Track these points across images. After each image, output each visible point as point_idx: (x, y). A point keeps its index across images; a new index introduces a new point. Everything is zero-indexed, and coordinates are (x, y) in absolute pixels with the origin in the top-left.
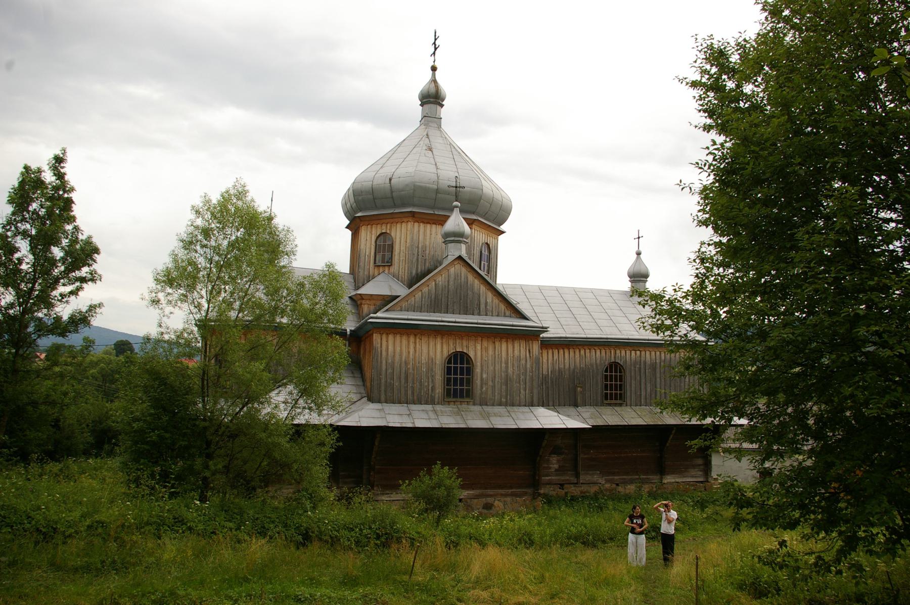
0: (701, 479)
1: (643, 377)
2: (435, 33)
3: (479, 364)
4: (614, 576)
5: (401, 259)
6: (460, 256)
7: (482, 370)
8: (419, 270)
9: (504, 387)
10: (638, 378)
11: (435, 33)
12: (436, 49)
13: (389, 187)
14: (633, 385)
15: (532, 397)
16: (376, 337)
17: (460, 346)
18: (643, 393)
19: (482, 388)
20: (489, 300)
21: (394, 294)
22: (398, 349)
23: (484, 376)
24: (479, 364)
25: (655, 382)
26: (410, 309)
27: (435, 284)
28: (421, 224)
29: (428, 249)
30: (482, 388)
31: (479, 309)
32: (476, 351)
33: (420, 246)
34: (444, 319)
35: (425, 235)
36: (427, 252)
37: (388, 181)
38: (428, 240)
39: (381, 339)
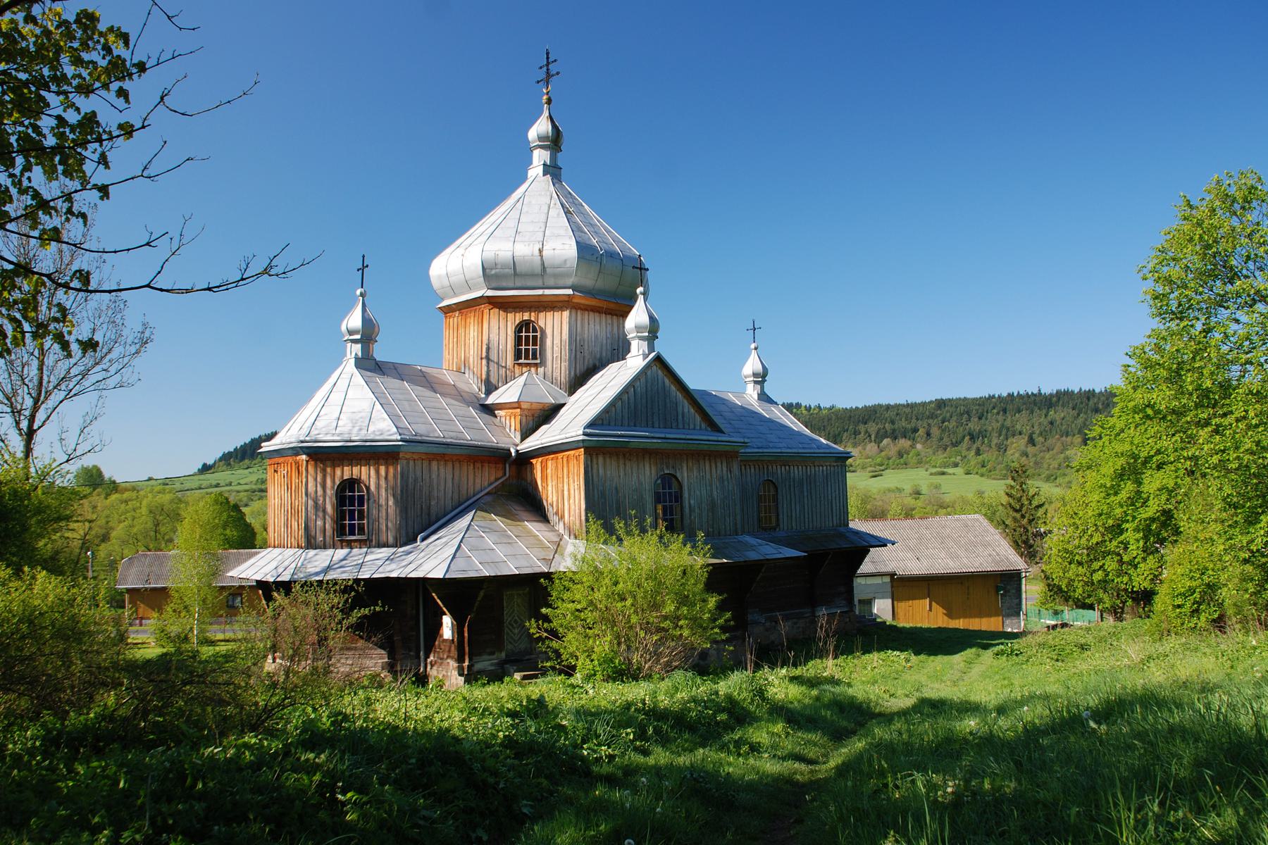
2: (548, 54)
3: (686, 484)
4: (759, 743)
5: (555, 356)
7: (690, 495)
8: (578, 371)
9: (710, 514)
11: (548, 54)
12: (549, 75)
13: (511, 253)
15: (736, 524)
16: (537, 463)
17: (347, 472)
18: (794, 515)
19: (690, 516)
20: (686, 410)
23: (692, 502)
24: (686, 484)
26: (613, 423)
29: (586, 343)
30: (690, 516)
32: (687, 475)
33: (578, 338)
36: (586, 347)
38: (586, 332)
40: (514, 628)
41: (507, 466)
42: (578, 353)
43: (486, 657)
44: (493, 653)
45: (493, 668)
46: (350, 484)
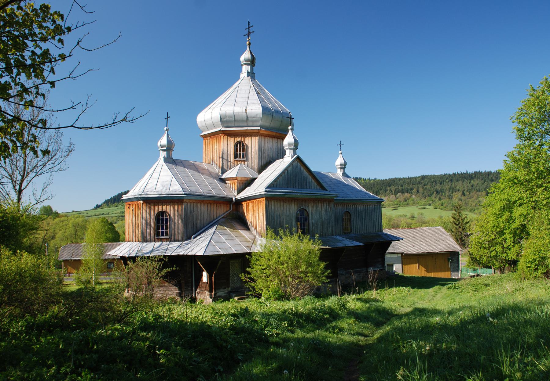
0: (381, 269)
1: (358, 220)
2: (249, 23)
4: (343, 328)
6: (46, 120)
10: (356, 219)
11: (249, 23)
14: (354, 223)
21: (254, 177)
22: (367, 208)
23: (313, 221)
25: (363, 221)
27: (288, 172)
28: (279, 139)
31: (307, 185)
32: (311, 209)
34: (302, 192)
35: (264, 144)
36: (266, 153)
37: (244, 111)
39: (269, 203)
40: (235, 277)
41: (231, 205)
42: (263, 155)
43: (222, 290)
44: (225, 288)
45: (225, 295)
46: (162, 214)
